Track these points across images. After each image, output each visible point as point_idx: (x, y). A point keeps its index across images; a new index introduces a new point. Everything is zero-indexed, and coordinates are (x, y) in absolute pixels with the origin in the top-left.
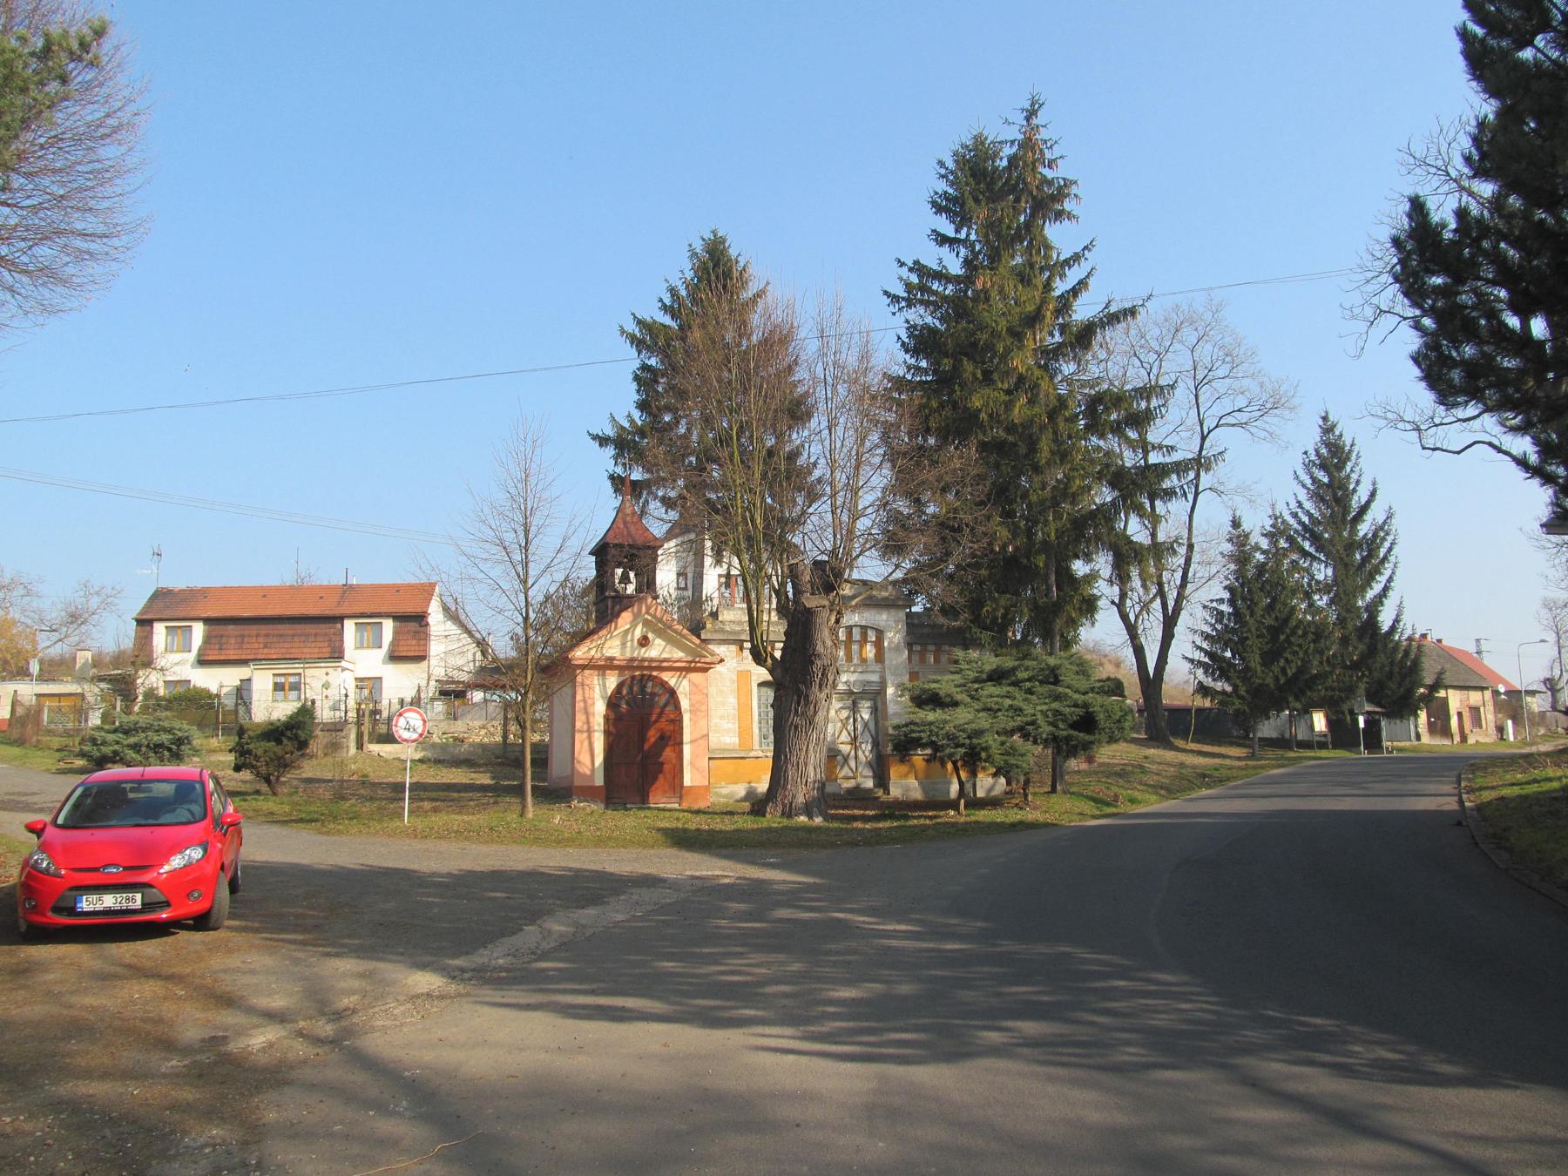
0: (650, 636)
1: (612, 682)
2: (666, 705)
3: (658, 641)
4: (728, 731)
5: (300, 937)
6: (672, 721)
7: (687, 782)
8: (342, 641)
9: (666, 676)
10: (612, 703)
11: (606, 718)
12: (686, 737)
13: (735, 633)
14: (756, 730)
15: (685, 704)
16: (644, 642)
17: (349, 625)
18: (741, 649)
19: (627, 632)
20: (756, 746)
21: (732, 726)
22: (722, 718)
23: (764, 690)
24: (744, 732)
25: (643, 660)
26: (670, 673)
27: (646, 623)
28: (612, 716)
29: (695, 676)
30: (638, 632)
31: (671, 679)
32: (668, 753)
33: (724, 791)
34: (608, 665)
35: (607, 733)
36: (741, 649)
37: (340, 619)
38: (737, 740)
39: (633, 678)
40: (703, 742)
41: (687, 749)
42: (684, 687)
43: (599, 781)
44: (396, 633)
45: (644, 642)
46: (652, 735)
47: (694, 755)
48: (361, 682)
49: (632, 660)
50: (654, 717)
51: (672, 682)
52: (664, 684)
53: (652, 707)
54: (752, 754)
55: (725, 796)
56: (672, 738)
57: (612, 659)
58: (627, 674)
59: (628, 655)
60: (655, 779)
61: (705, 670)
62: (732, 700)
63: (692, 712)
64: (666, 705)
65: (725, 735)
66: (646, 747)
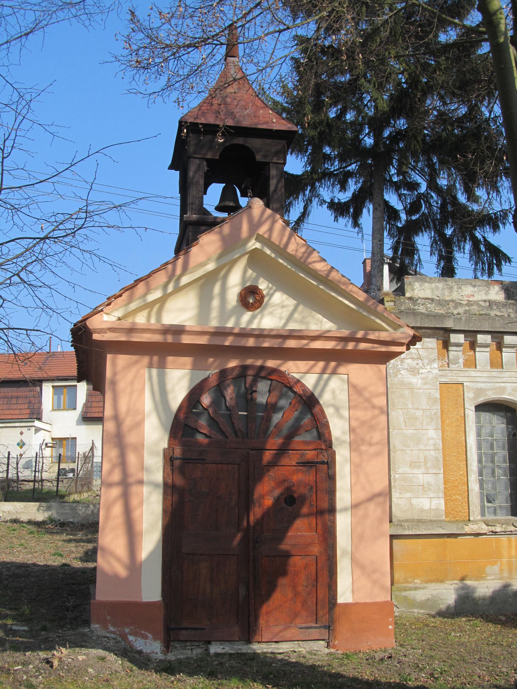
0: (263, 285)
1: (179, 380)
2: (294, 431)
3: (278, 297)
4: (425, 488)
5: (407, 475)
6: (308, 464)
7: (345, 594)
8: (40, 403)
9: (294, 369)
10: (181, 427)
11: (169, 459)
12: (343, 496)
13: (436, 316)
14: (474, 486)
15: (338, 428)
16: (251, 298)
17: (47, 389)
18: (446, 345)
19: (209, 279)
20: (475, 515)
21: (432, 478)
22: (413, 464)
23: (486, 416)
24: (453, 489)
25: (244, 334)
26: (303, 365)
27: (255, 259)
28: (178, 452)
29: (359, 372)
30: (235, 282)
31: (306, 375)
32: (301, 531)
33: (421, 595)
34: (167, 346)
35: (169, 489)
36: (446, 345)
37: (39, 382)
38: (439, 504)
39: (223, 374)
40: (374, 510)
41: (343, 523)
42: (335, 392)
43: (151, 591)
44: (89, 395)
45: (251, 298)
46: (266, 494)
47: (358, 538)
48: (58, 442)
49: (221, 333)
50: (268, 456)
51: (309, 381)
52: (286, 385)
53: (264, 431)
54: (467, 529)
55: (422, 605)
56: (311, 500)
57: (178, 330)
58: (211, 371)
59: (214, 323)
60: (272, 588)
61: (384, 358)
62: (433, 434)
63: (354, 446)
64: (294, 431)
65: (422, 498)
66: (256, 513)
